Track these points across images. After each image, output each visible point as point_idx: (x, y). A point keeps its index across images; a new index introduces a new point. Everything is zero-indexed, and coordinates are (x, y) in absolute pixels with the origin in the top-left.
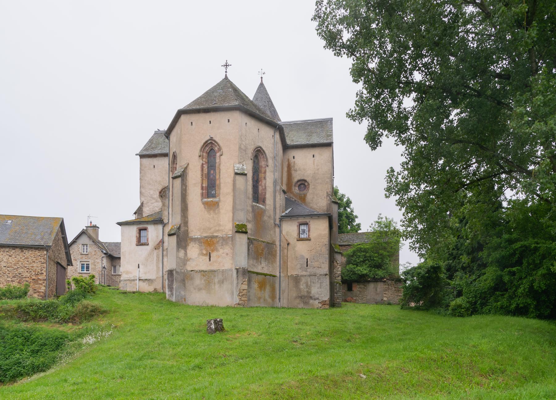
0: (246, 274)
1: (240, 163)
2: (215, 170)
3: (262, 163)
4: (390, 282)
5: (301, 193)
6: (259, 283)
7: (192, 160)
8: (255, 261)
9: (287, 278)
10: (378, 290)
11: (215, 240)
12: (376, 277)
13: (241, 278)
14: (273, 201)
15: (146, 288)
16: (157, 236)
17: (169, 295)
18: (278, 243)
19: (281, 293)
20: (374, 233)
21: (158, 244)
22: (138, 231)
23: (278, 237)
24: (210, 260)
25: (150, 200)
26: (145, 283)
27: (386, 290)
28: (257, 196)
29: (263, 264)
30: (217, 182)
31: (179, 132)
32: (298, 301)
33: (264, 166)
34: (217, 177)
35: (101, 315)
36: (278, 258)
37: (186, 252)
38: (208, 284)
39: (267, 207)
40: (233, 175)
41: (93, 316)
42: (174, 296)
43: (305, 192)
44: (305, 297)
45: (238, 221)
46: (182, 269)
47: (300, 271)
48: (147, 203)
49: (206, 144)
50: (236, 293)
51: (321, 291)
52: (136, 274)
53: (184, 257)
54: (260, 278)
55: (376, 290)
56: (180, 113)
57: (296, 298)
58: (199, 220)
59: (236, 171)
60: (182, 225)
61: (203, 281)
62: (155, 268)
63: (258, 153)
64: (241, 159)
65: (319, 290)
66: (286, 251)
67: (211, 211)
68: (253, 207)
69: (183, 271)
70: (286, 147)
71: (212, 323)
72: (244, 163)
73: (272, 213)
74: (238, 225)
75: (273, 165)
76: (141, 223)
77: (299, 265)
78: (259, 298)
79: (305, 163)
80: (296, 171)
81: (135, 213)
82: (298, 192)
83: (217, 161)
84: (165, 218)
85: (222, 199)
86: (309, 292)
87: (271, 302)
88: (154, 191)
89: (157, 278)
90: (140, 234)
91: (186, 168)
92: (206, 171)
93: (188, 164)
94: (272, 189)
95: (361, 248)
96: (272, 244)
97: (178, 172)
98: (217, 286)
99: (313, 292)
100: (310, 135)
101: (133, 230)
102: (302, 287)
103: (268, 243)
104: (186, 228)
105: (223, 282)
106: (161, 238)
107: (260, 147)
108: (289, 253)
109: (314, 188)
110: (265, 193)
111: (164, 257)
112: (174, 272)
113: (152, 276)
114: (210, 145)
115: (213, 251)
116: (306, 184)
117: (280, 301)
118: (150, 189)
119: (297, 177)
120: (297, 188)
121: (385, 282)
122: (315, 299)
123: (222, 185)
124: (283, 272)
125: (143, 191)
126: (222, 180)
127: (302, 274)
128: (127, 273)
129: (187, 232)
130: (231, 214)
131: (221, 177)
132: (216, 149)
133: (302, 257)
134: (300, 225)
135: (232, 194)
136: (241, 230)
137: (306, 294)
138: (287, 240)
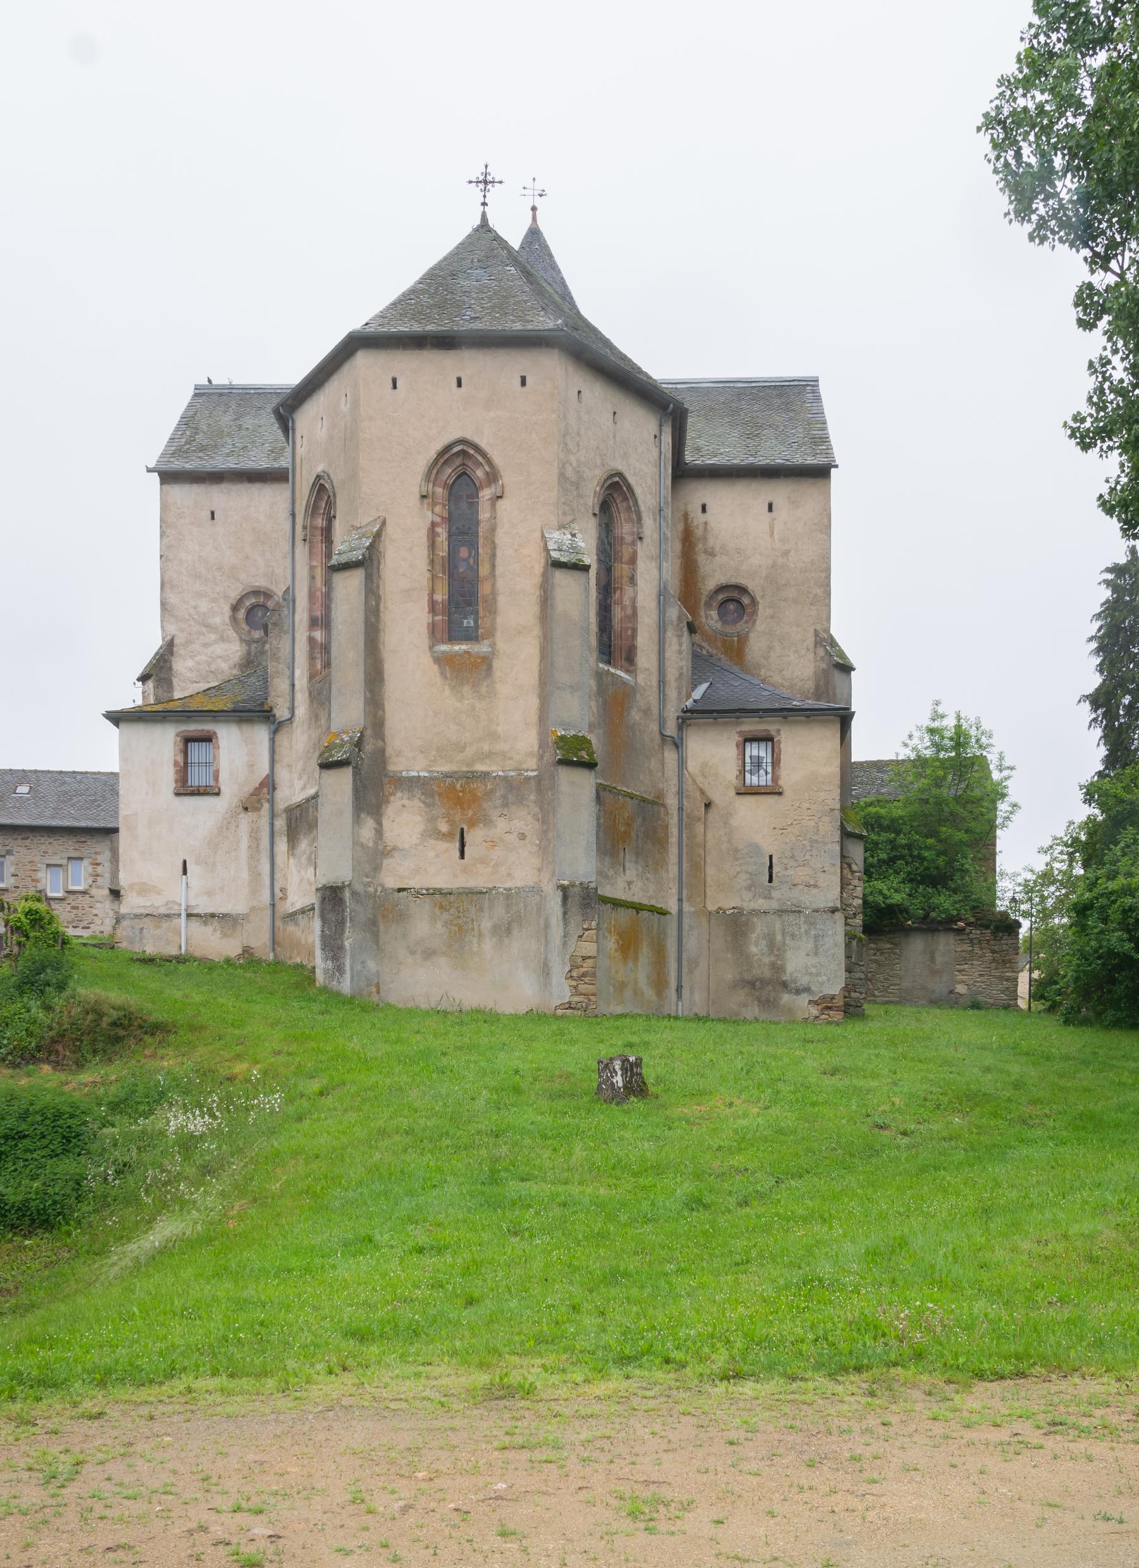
0: (583, 900)
1: (561, 527)
2: (473, 545)
3: (624, 529)
4: (976, 933)
5: (730, 629)
6: (621, 935)
7: (395, 507)
8: (607, 860)
9: (704, 920)
10: (939, 959)
11: (479, 788)
12: (933, 914)
13: (576, 918)
14: (660, 656)
15: (215, 944)
16: (251, 766)
17: (326, 971)
18: (672, 801)
19: (685, 970)
20: (920, 763)
21: (257, 792)
22: (181, 746)
23: (675, 781)
24: (462, 856)
25: (200, 633)
26: (209, 929)
27: (965, 961)
28: (613, 644)
29: (632, 872)
30: (485, 589)
31: (344, 408)
32: (741, 995)
33: (628, 539)
34: (484, 571)
35: (148, 1039)
36: (673, 850)
37: (380, 823)
38: (459, 935)
39: (641, 679)
40: (538, 567)
41: (118, 1040)
42: (348, 975)
43: (741, 626)
44: (765, 982)
45: (565, 726)
46: (368, 884)
47: (747, 895)
48: (189, 642)
49: (446, 456)
50: (559, 970)
51: (818, 960)
52: (176, 894)
53: (376, 843)
54: (624, 917)
55: (932, 959)
56: (354, 345)
57: (735, 986)
58: (423, 715)
59: (555, 555)
60: (368, 733)
61: (439, 925)
62: (245, 875)
63: (615, 493)
64: (564, 514)
65: (812, 960)
66: (699, 828)
67: (466, 689)
68: (599, 676)
69: (371, 889)
70: (683, 473)
71: (617, 1067)
72: (576, 527)
73: (651, 697)
74: (562, 738)
75: (656, 536)
76: (167, 707)
77: (743, 876)
78: (622, 986)
79: (741, 527)
80: (712, 554)
81: (144, 678)
82: (718, 626)
83: (484, 515)
84: (280, 701)
85: (501, 645)
86: (778, 968)
87: (654, 998)
88: (214, 600)
89: (253, 909)
90: (185, 753)
91: (378, 535)
92: (443, 551)
93: (384, 523)
94: (655, 617)
95: (878, 818)
96: (653, 803)
97: (345, 544)
98: (488, 944)
99: (791, 967)
100: (753, 431)
101: (163, 741)
102: (754, 949)
103: (644, 800)
104: (380, 743)
105: (509, 931)
106: (265, 770)
107: (620, 474)
108: (709, 835)
109: (772, 617)
110: (634, 631)
111: (277, 839)
112: (347, 895)
113: (236, 905)
114: (458, 461)
115: (472, 824)
116: (746, 600)
117: (679, 996)
118: (200, 595)
119: (715, 574)
120: (714, 613)
121: (960, 931)
122: (798, 992)
123: (502, 600)
124: (689, 898)
125: (173, 599)
126: (500, 584)
127: (754, 905)
128: (144, 889)
129: (381, 757)
130: (534, 702)
131: (499, 570)
132: (480, 473)
133: (755, 849)
134: (746, 740)
135: (536, 631)
136: (573, 755)
137: (767, 974)
138: (702, 792)
